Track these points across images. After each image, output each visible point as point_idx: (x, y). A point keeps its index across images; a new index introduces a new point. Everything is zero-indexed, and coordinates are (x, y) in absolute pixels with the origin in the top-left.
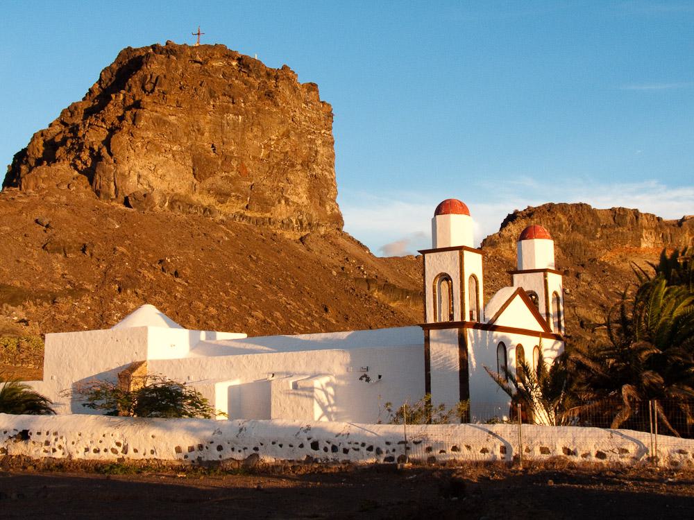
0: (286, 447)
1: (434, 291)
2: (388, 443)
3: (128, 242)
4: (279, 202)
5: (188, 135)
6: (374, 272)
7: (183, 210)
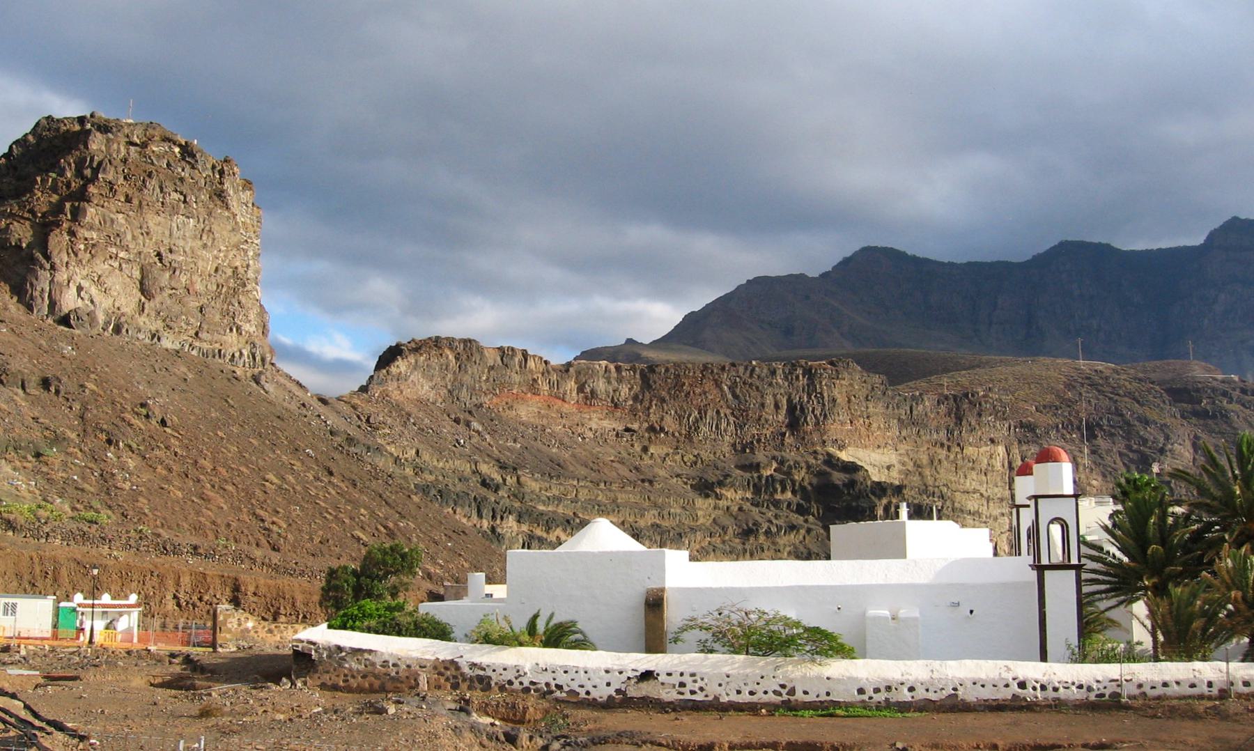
2: (1098, 681)
3: (93, 376)
4: (231, 330)
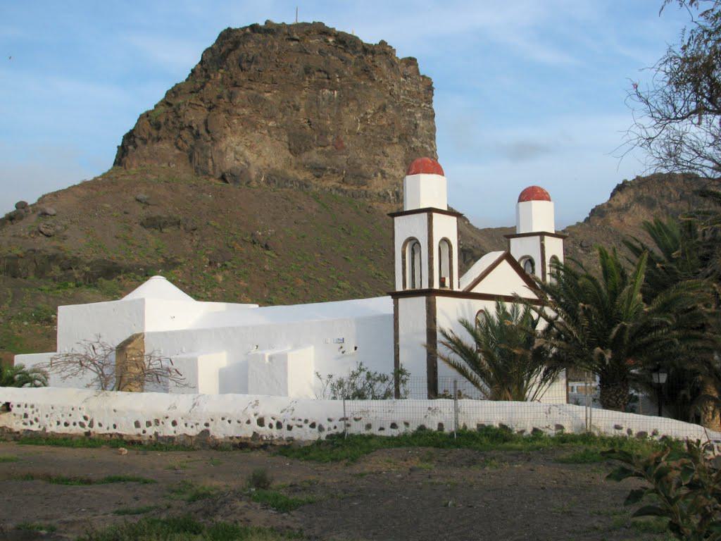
0: (234, 422)
1: (404, 257)
2: (330, 420)
4: (376, 175)
5: (283, 110)
6: (471, 243)
7: (279, 184)
